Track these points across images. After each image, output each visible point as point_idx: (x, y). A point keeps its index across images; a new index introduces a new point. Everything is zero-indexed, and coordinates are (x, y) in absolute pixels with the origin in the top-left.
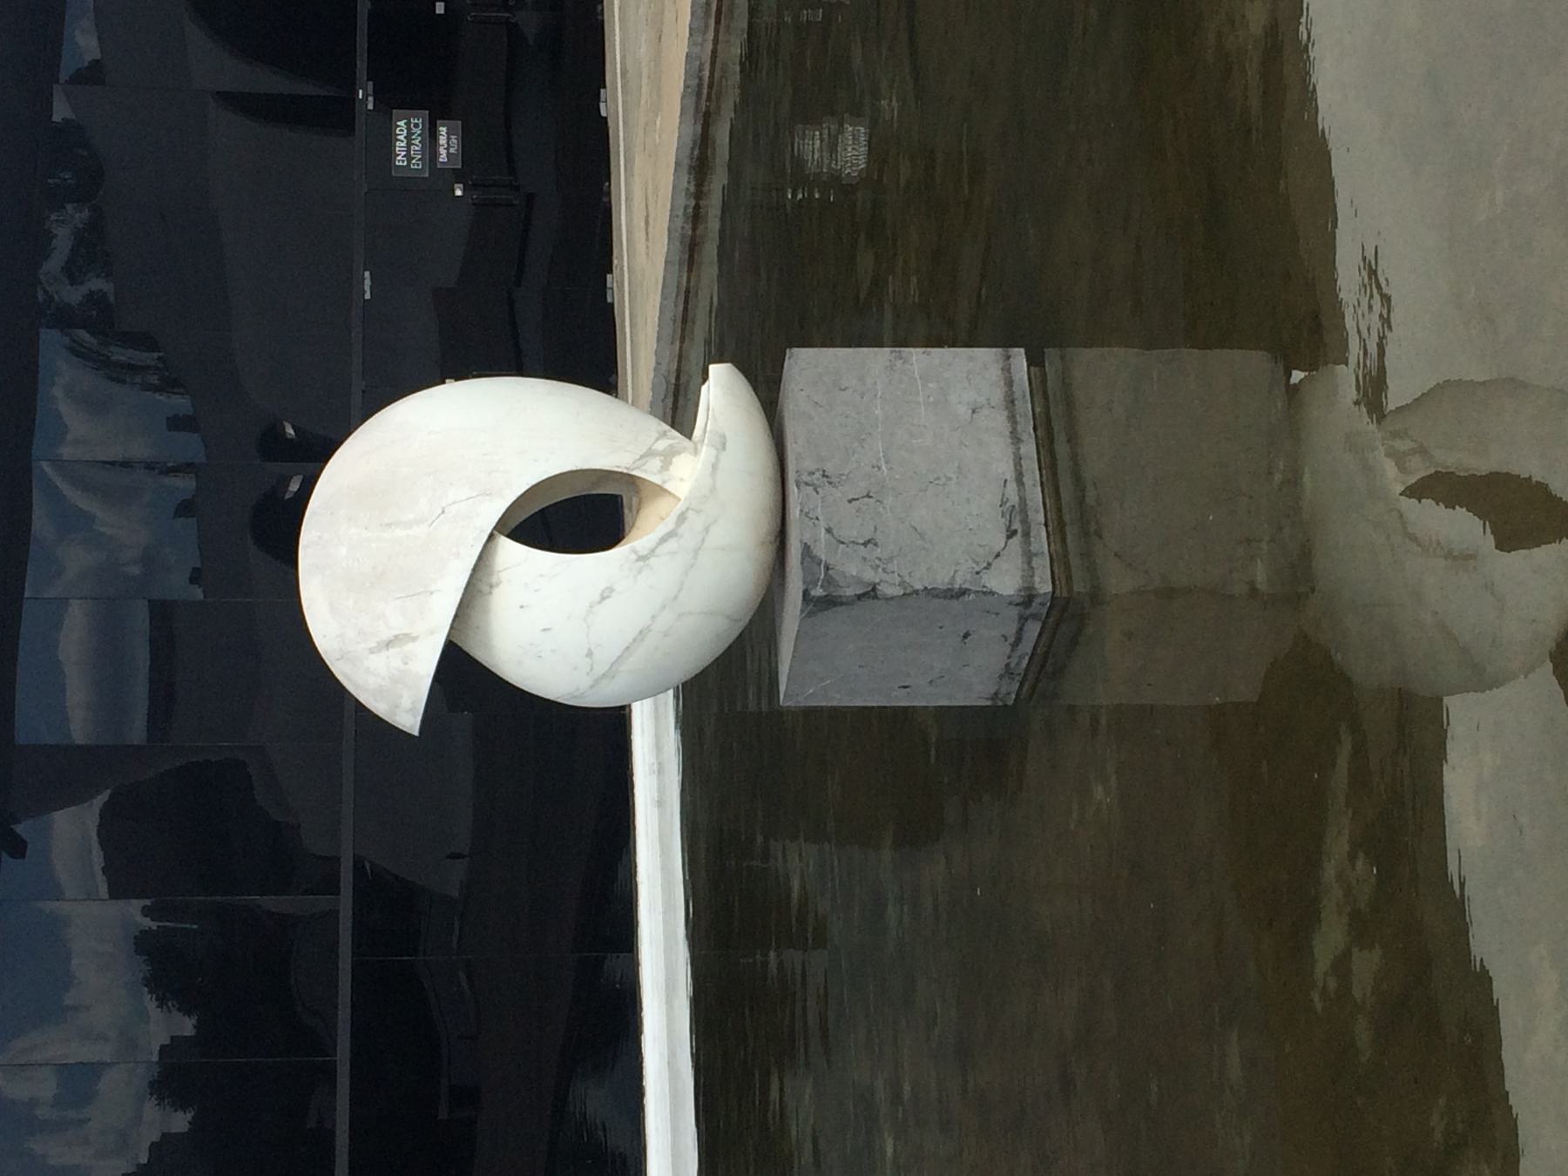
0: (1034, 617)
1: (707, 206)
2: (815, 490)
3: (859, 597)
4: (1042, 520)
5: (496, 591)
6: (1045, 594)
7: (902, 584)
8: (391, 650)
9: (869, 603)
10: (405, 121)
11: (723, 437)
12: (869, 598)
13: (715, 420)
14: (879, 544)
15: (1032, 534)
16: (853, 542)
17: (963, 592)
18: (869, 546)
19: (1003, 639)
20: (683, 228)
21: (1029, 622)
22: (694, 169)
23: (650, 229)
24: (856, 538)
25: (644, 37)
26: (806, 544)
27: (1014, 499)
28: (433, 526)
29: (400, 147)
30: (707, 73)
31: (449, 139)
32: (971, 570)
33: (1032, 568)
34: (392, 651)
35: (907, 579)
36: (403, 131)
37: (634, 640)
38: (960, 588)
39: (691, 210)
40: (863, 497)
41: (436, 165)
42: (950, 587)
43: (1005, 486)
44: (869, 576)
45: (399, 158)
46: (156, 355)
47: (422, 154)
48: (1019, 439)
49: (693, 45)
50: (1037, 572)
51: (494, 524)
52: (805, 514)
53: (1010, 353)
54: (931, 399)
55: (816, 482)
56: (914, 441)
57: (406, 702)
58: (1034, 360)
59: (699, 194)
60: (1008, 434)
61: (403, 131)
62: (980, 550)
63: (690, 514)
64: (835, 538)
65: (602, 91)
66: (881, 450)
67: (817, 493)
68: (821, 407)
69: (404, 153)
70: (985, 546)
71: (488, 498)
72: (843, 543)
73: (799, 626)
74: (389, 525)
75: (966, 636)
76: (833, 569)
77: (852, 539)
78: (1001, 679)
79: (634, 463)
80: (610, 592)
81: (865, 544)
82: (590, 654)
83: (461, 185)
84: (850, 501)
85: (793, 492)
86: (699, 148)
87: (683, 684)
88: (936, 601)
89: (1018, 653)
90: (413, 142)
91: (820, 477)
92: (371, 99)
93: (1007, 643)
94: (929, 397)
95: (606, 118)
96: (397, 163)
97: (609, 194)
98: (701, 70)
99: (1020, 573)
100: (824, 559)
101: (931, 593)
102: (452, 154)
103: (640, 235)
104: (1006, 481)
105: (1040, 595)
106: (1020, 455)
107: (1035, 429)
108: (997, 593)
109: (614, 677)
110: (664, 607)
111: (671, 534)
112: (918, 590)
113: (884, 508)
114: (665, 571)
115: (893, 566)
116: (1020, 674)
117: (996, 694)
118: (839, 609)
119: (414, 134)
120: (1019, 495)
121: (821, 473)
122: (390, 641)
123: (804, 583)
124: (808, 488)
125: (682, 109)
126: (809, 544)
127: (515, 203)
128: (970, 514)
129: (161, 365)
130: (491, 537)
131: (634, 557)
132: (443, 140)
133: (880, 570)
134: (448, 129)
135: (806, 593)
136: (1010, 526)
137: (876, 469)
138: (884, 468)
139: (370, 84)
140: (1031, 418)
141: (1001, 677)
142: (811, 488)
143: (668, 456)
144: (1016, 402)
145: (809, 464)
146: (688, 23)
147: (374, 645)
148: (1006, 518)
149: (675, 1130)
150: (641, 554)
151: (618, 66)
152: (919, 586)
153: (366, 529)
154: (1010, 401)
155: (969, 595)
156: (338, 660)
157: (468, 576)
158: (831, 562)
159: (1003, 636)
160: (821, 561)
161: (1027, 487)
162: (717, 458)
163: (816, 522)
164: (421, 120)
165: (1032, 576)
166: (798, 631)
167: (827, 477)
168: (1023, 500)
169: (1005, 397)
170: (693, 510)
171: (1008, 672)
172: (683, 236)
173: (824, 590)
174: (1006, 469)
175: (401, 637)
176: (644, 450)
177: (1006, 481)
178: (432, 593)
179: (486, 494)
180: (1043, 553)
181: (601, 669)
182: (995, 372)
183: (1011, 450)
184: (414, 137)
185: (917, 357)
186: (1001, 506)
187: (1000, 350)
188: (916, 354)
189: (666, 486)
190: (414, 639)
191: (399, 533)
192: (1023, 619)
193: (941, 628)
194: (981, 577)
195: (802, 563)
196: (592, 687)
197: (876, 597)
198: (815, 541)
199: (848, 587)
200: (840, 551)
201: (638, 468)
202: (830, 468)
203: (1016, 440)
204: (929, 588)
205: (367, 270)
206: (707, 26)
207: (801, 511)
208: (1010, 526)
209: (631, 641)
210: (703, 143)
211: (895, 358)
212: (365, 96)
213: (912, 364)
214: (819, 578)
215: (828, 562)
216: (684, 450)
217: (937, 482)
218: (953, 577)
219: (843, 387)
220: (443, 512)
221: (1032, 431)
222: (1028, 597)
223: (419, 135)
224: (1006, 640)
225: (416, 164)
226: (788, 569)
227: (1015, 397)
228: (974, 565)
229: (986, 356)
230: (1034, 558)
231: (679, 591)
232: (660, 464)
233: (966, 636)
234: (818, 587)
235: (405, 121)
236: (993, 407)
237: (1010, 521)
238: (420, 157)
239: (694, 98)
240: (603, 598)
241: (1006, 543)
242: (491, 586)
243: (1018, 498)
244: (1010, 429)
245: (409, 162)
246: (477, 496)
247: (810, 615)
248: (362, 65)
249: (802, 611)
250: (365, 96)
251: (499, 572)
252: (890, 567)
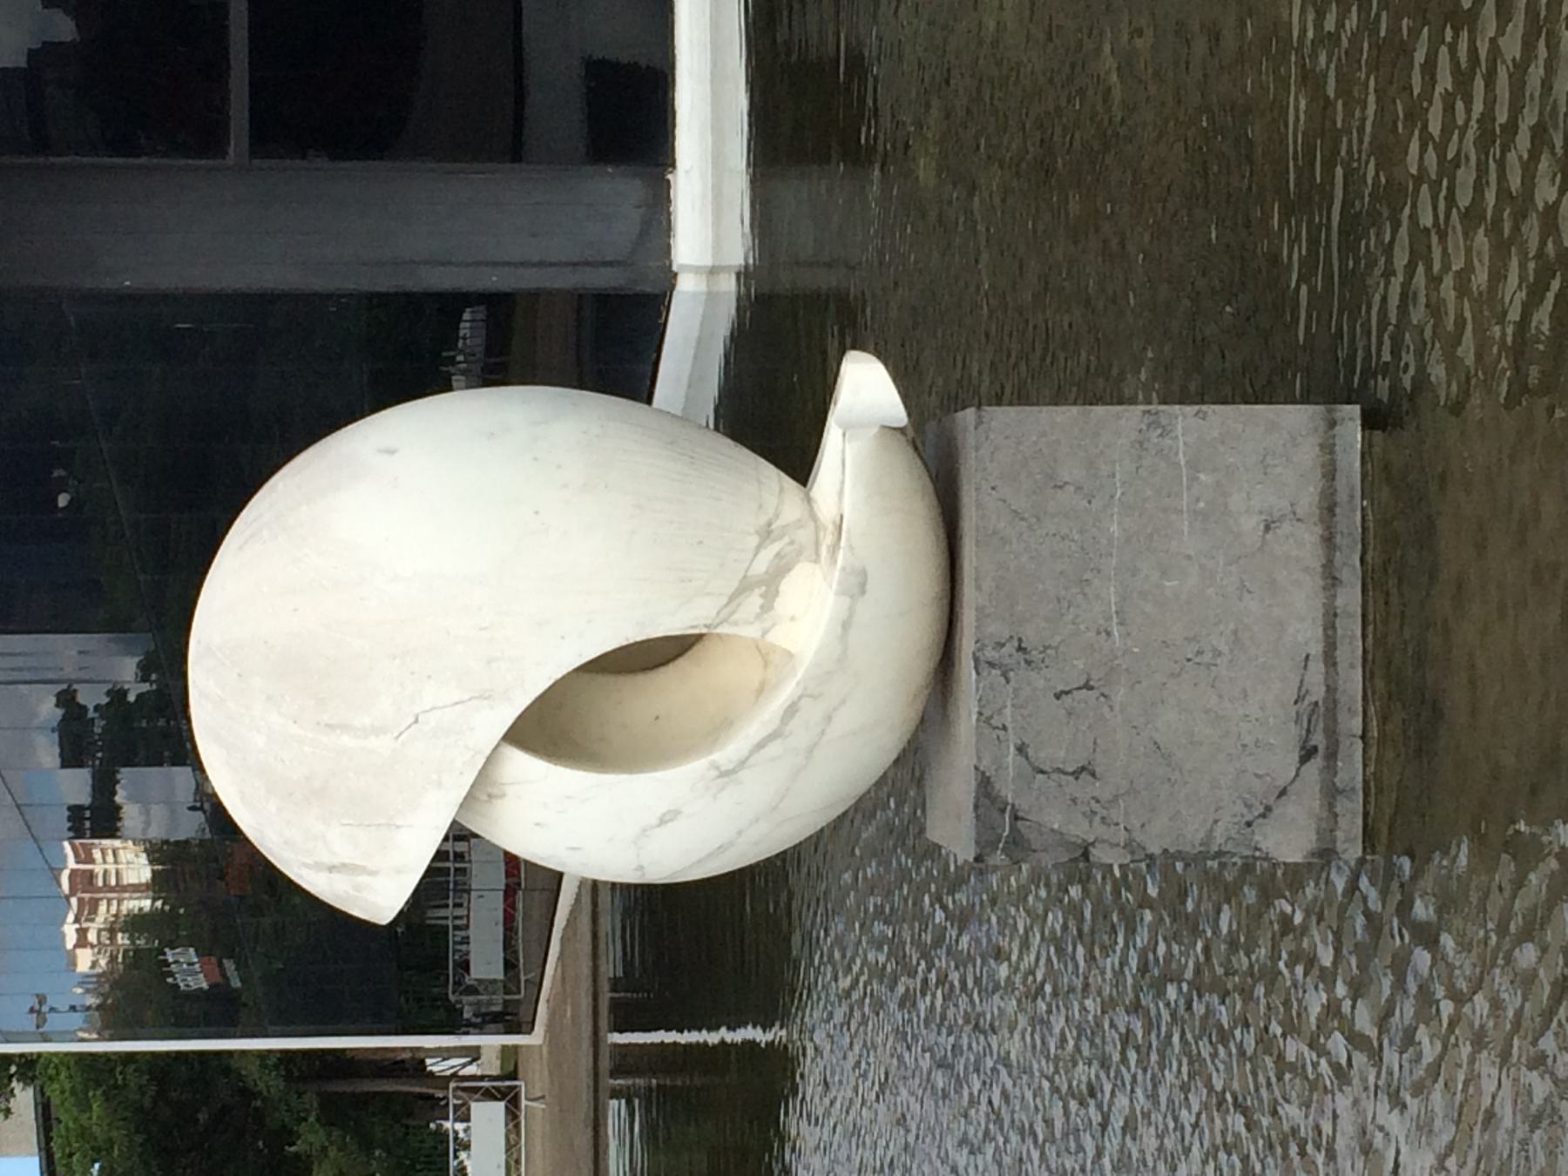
2: (1005, 675)
7: (1129, 845)
15: (1339, 757)
16: (1058, 769)
18: (1084, 775)
27: (1318, 693)
28: (401, 739)
32: (1239, 818)
33: (1336, 815)
35: (1139, 837)
44: (1080, 830)
48: (1334, 578)
50: (1342, 822)
52: (984, 719)
53: (1338, 415)
54: (1202, 505)
55: (1007, 661)
58: (1371, 421)
60: (1320, 569)
62: (1256, 783)
64: (1030, 764)
68: (1023, 519)
71: (486, 702)
72: (1042, 772)
74: (330, 726)
77: (1055, 766)
79: (718, 613)
81: (1076, 774)
84: (1058, 696)
94: (1198, 500)
100: (1010, 801)
106: (1335, 608)
110: (757, 820)
113: (1111, 708)
114: (757, 788)
115: (1116, 814)
123: (977, 843)
131: (714, 773)
133: (1097, 819)
136: (1306, 741)
144: (1338, 510)
145: (996, 629)
149: (716, 48)
150: (723, 769)
154: (1329, 508)
158: (1023, 804)
161: (1339, 669)
162: (852, 611)
163: (1002, 733)
170: (808, 696)
174: (1309, 636)
176: (736, 584)
177: (1307, 657)
178: (398, 827)
179: (485, 697)
180: (1353, 789)
182: (1308, 454)
183: (1319, 602)
185: (1183, 417)
186: (1296, 702)
187: (1320, 408)
188: (1185, 417)
191: (347, 740)
194: (1253, 833)
198: (1000, 767)
201: (725, 620)
202: (1030, 635)
203: (1329, 581)
204: (1172, 851)
207: (980, 714)
211: (1149, 426)
214: (1000, 836)
218: (1211, 830)
220: (416, 721)
221: (1358, 563)
227: (1338, 500)
228: (1245, 811)
229: (1297, 418)
237: (1308, 731)
240: (663, 821)
243: (1323, 689)
246: (470, 699)
252: (1116, 814)
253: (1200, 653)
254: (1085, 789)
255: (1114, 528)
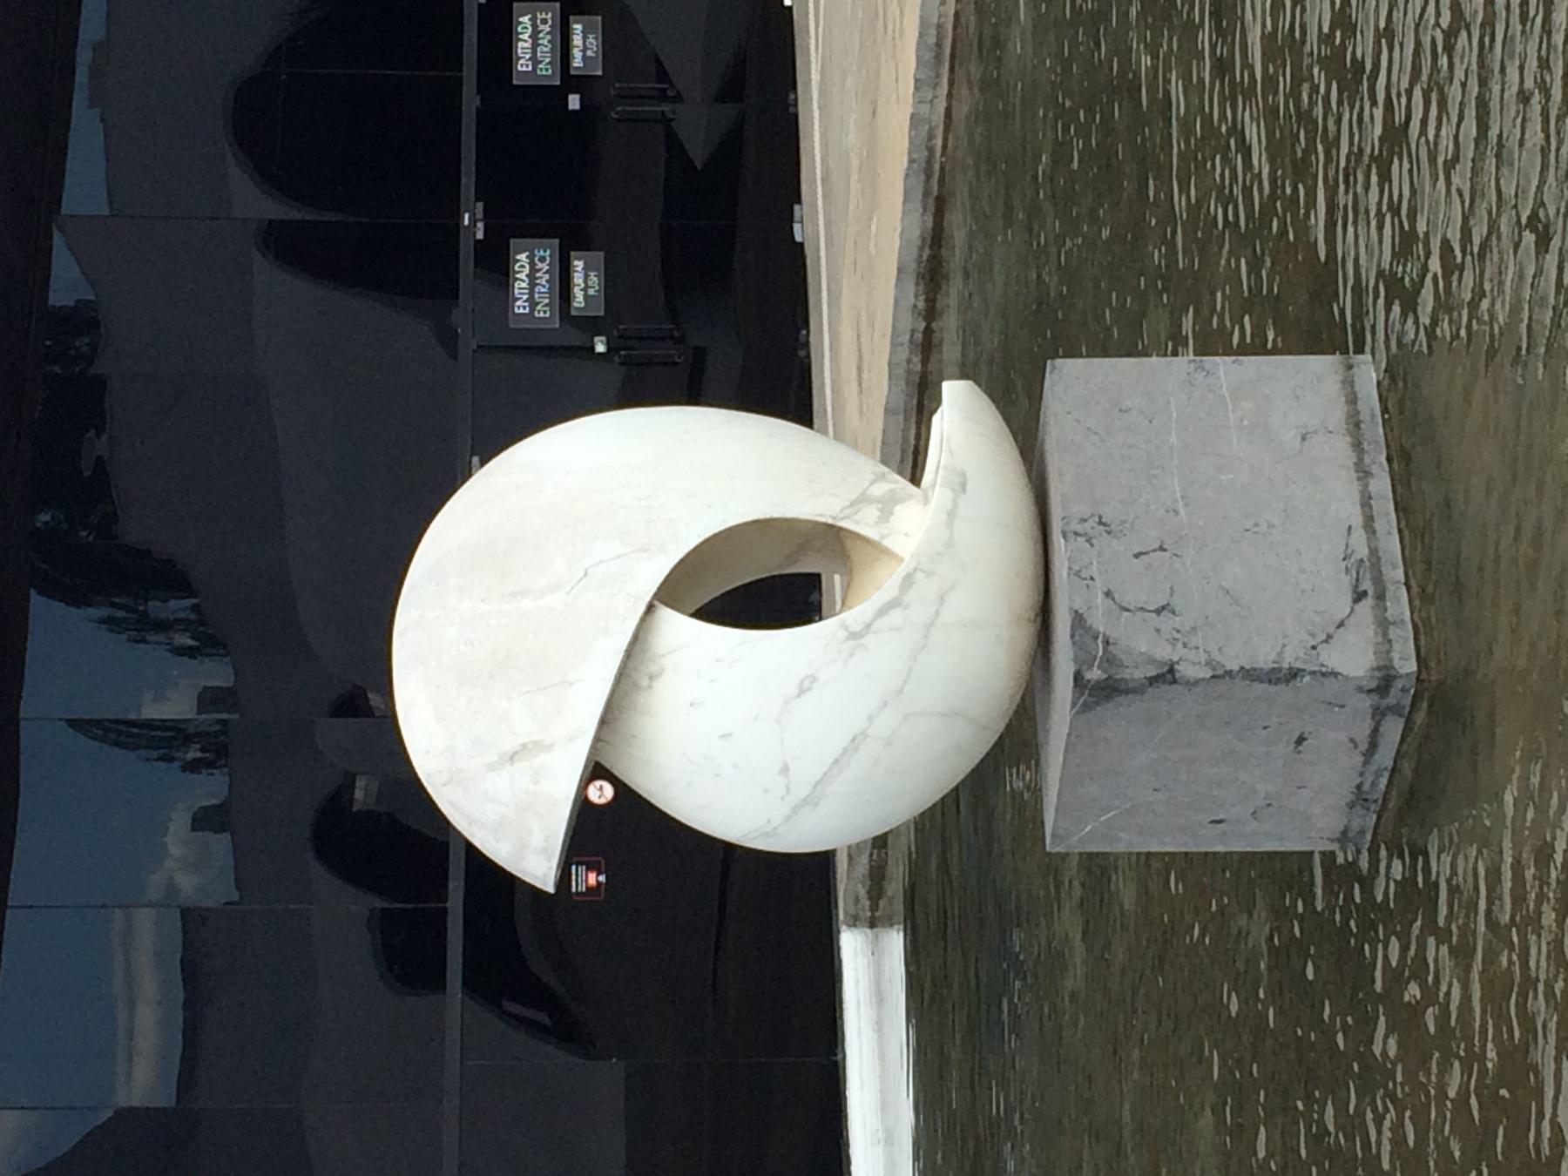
0: (1395, 710)
1: (942, 330)
2: (1089, 541)
3: (1153, 681)
4: (1402, 578)
5: (657, 684)
6: (1407, 674)
8: (516, 764)
9: (1165, 688)
10: (530, 16)
11: (963, 474)
12: (1164, 682)
13: (951, 452)
14: (1177, 610)
17: (1294, 674)
18: (1164, 613)
19: (1351, 745)
20: (909, 361)
21: (1387, 718)
22: (923, 278)
23: (865, 376)
24: (1146, 603)
25: (853, 116)
26: (1076, 612)
27: (1363, 552)
29: (520, 289)
30: (939, 142)
31: (586, 277)
33: (1390, 641)
34: (520, 766)
36: (526, 28)
37: (845, 750)
38: (1291, 668)
39: (920, 335)
40: (1154, 551)
41: (569, 312)
42: (1276, 665)
43: (1349, 534)
44: (1164, 652)
45: (518, 303)
46: (188, 602)
47: (550, 298)
49: (920, 102)
50: (1396, 646)
51: (654, 590)
55: (1090, 531)
56: (1223, 477)
57: (537, 840)
59: (931, 313)
61: (526, 28)
63: (919, 576)
65: (797, 207)
66: (1178, 489)
67: (1092, 545)
69: (525, 297)
70: (1324, 612)
72: (1127, 610)
73: (1071, 728)
74: (513, 595)
75: (1301, 740)
76: (1115, 644)
77: (1140, 606)
78: (1351, 808)
79: (842, 511)
80: (812, 683)
81: (1158, 611)
82: (785, 770)
83: (603, 338)
84: (1137, 556)
85: (1060, 543)
86: (931, 247)
87: (916, 823)
88: (1258, 686)
89: (1373, 767)
90: (538, 281)
91: (1095, 525)
92: (480, 225)
93: (1357, 752)
95: (802, 245)
96: (516, 310)
97: (807, 345)
98: (931, 137)
99: (1371, 650)
101: (1252, 675)
102: (592, 296)
103: (851, 390)
104: (1350, 528)
105: (1401, 676)
107: (1389, 460)
108: (1341, 674)
109: (817, 804)
110: (885, 704)
111: (894, 604)
112: (1231, 671)
116: (1376, 801)
117: (1345, 833)
118: (1121, 699)
119: (541, 31)
120: (1369, 547)
121: (1097, 519)
122: (516, 753)
124: (1079, 539)
125: (906, 192)
126: (1080, 611)
127: (678, 361)
128: (1302, 571)
129: (193, 617)
130: (650, 608)
132: (577, 40)
133: (1180, 645)
134: (585, 264)
135: (1078, 677)
136: (1356, 586)
137: (1172, 513)
138: (1182, 512)
139: (480, 205)
140: (1384, 446)
141: (1351, 805)
142: (1083, 539)
143: (887, 507)
144: (1362, 426)
145: (1080, 509)
146: (912, 72)
147: (494, 758)
148: (1352, 576)
151: (818, 166)
152: (1234, 666)
153: (483, 600)
154: (1354, 424)
155: (1303, 676)
156: (445, 784)
157: (618, 663)
158: (1113, 634)
159: (1352, 740)
160: (1099, 633)
163: (1090, 582)
164: (550, 15)
165: (1388, 652)
166: (1069, 735)
167: (1105, 524)
168: (1374, 551)
169: (1347, 419)
171: (1360, 797)
172: (909, 372)
173: (1104, 671)
175: (530, 746)
177: (1350, 528)
178: (571, 684)
180: (1403, 621)
181: (801, 791)
182: (1332, 386)
183: (1356, 487)
184: (538, 275)
186: (1344, 559)
189: (886, 543)
190: (549, 748)
192: (1379, 714)
193: (1265, 728)
195: (1072, 636)
196: (788, 818)
197: (1175, 681)
198: (1089, 608)
199: (1136, 667)
200: (1123, 620)
205: (476, 454)
206: (938, 76)
207: (1070, 568)
208: (1356, 586)
209: (840, 751)
210: (936, 238)
212: (473, 223)
213: (1219, 378)
215: (1107, 633)
216: (911, 497)
217: (1256, 529)
219: (1124, 409)
220: (586, 575)
222: (1385, 680)
223: (548, 33)
224: (1356, 747)
225: (542, 312)
226: (1054, 660)
228: (1309, 638)
230: (1391, 627)
231: (905, 682)
232: (878, 513)
233: (1301, 740)
234: (1095, 668)
235: (530, 16)
236: (1331, 432)
237: (1357, 580)
238: (547, 301)
239: (923, 177)
240: (802, 691)
241: (1352, 610)
242: (651, 678)
244: (1355, 460)
245: (532, 310)
247: (1086, 707)
248: (468, 182)
249: (1074, 704)
250: (473, 223)
251: (663, 656)
252: (1193, 641)
253: (1256, 525)
254: (1166, 622)
255: (1173, 439)
